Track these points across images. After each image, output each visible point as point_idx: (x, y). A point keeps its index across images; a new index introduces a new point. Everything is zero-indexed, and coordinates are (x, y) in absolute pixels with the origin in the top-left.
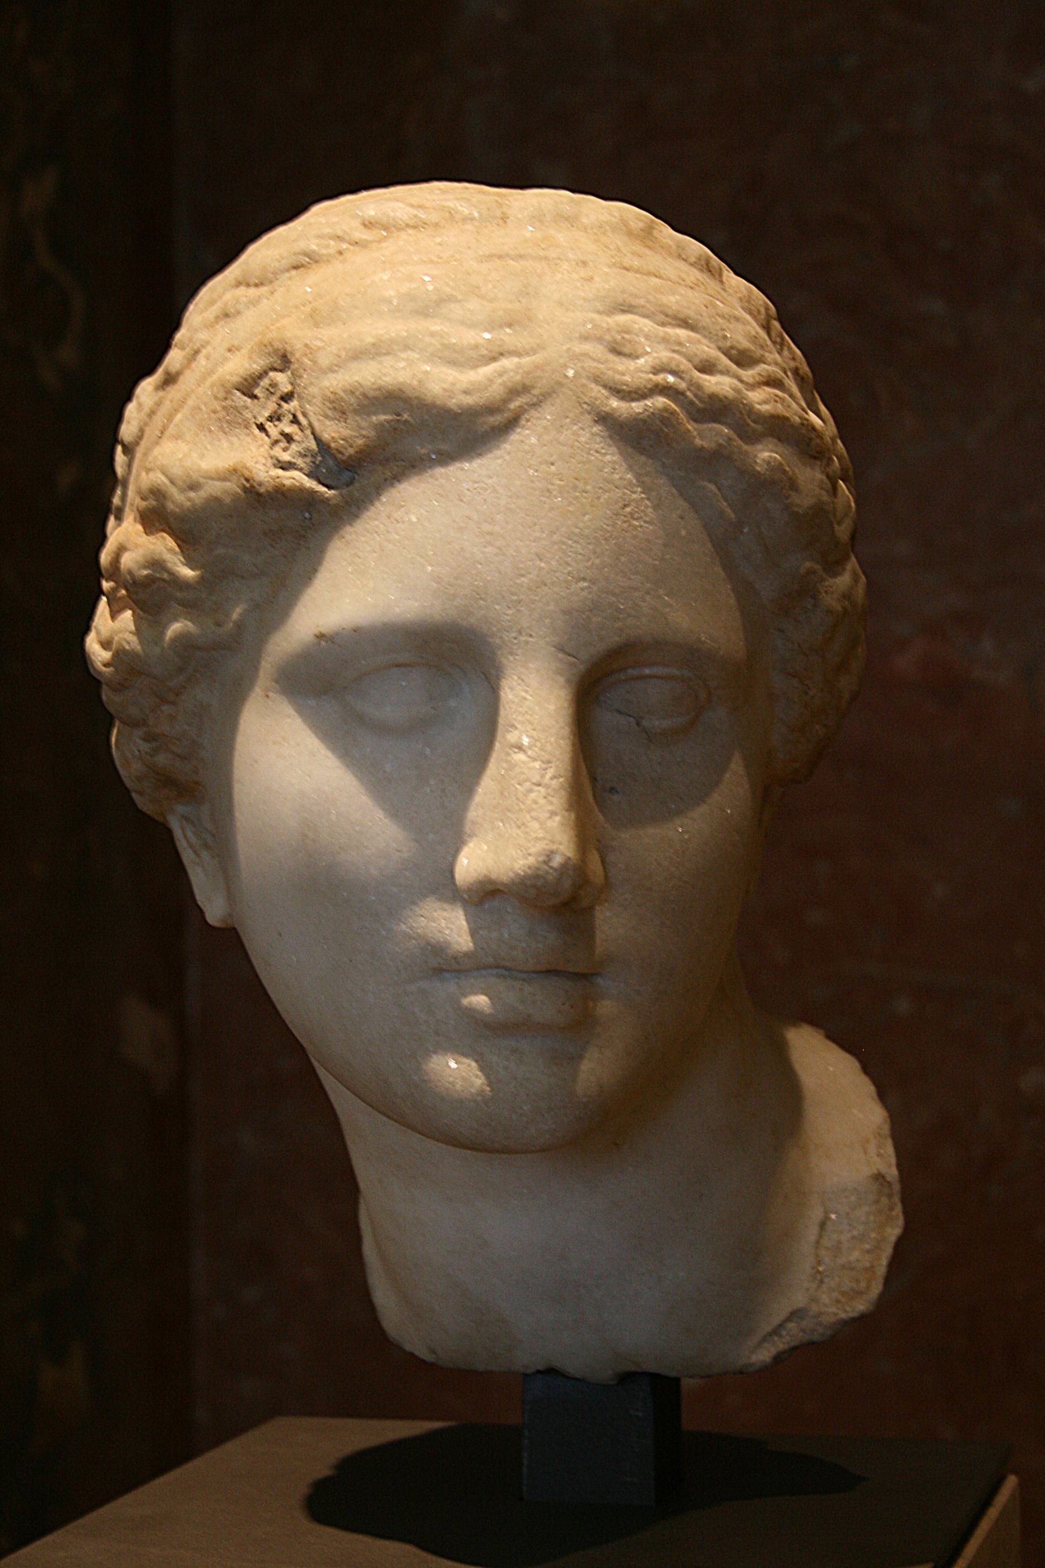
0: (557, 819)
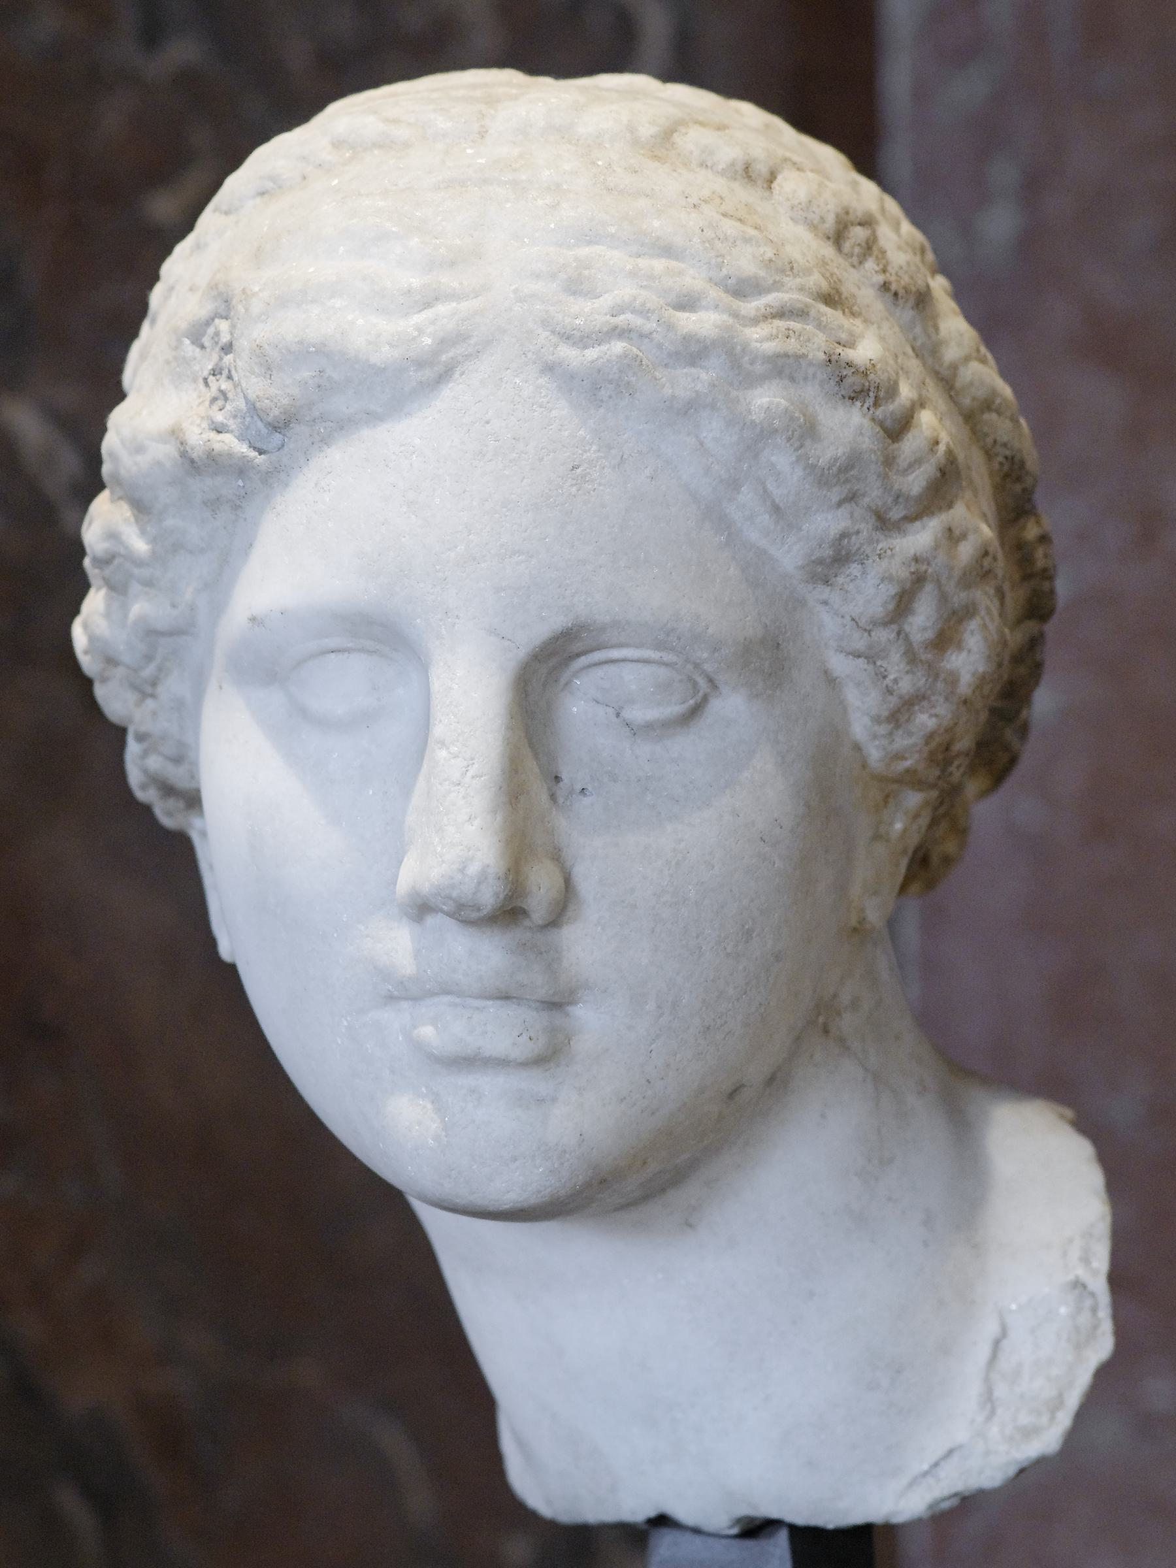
0: (477, 822)
